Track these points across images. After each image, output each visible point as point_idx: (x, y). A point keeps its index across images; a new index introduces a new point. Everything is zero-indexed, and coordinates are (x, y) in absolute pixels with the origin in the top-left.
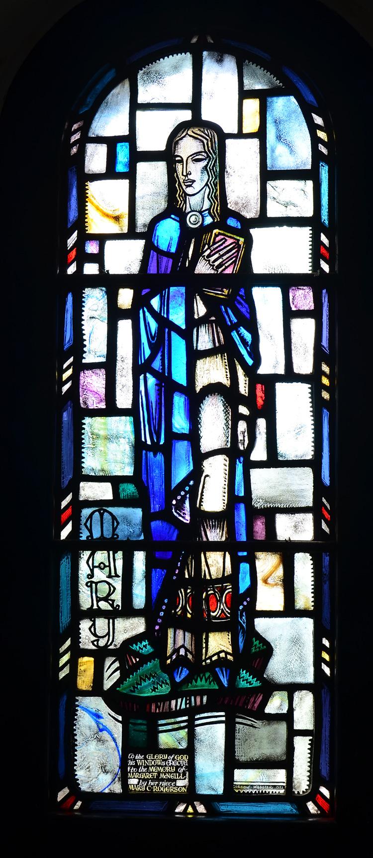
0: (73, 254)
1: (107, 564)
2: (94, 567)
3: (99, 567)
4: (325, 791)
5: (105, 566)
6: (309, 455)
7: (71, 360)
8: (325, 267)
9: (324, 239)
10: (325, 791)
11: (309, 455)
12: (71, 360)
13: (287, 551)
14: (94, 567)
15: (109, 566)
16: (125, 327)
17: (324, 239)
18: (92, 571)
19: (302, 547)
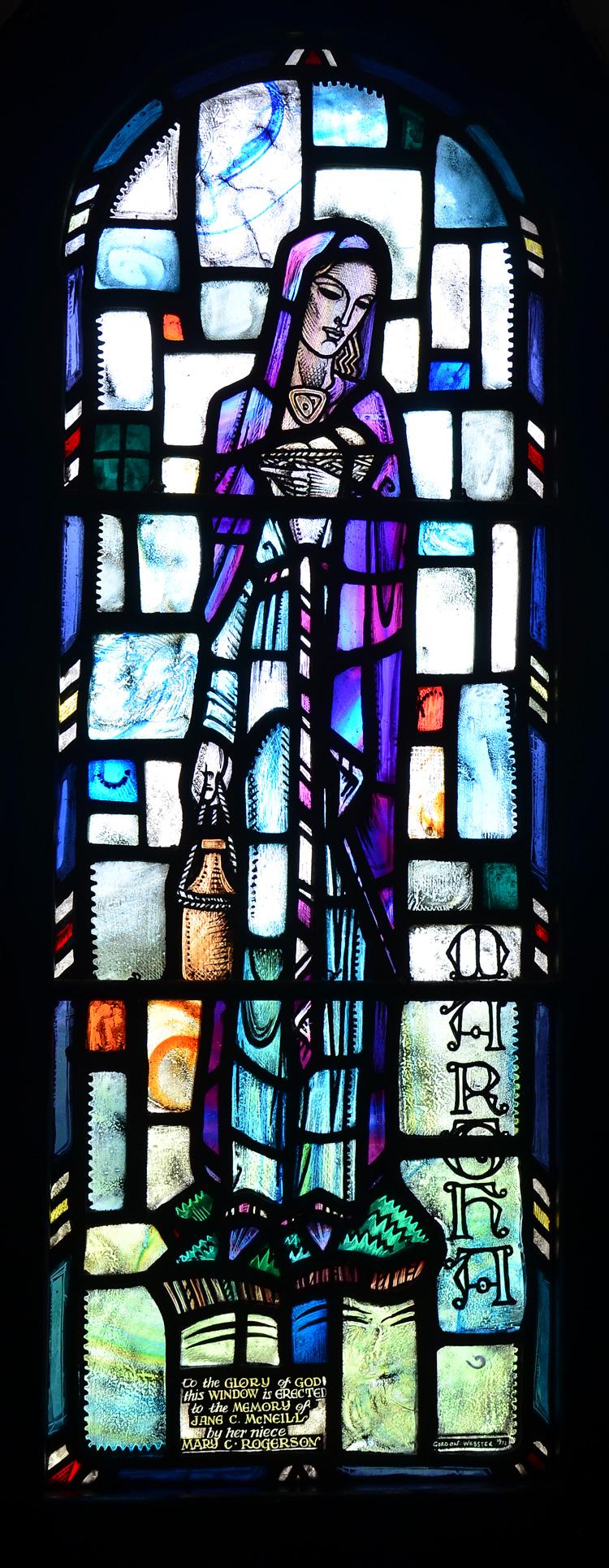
0: (73, 442)
1: (494, 1280)
2: (469, 1286)
3: (477, 1286)
4: (540, 910)
5: (489, 1284)
6: (94, 1299)
7: (308, 1007)
8: (535, 482)
9: (536, 433)
10: (540, 910)
11: (94, 1299)
12: (308, 1007)
13: (448, 845)
14: (469, 1286)
15: (498, 1284)
16: (403, 289)
17: (536, 433)
18: (465, 1293)
19: (429, 850)
